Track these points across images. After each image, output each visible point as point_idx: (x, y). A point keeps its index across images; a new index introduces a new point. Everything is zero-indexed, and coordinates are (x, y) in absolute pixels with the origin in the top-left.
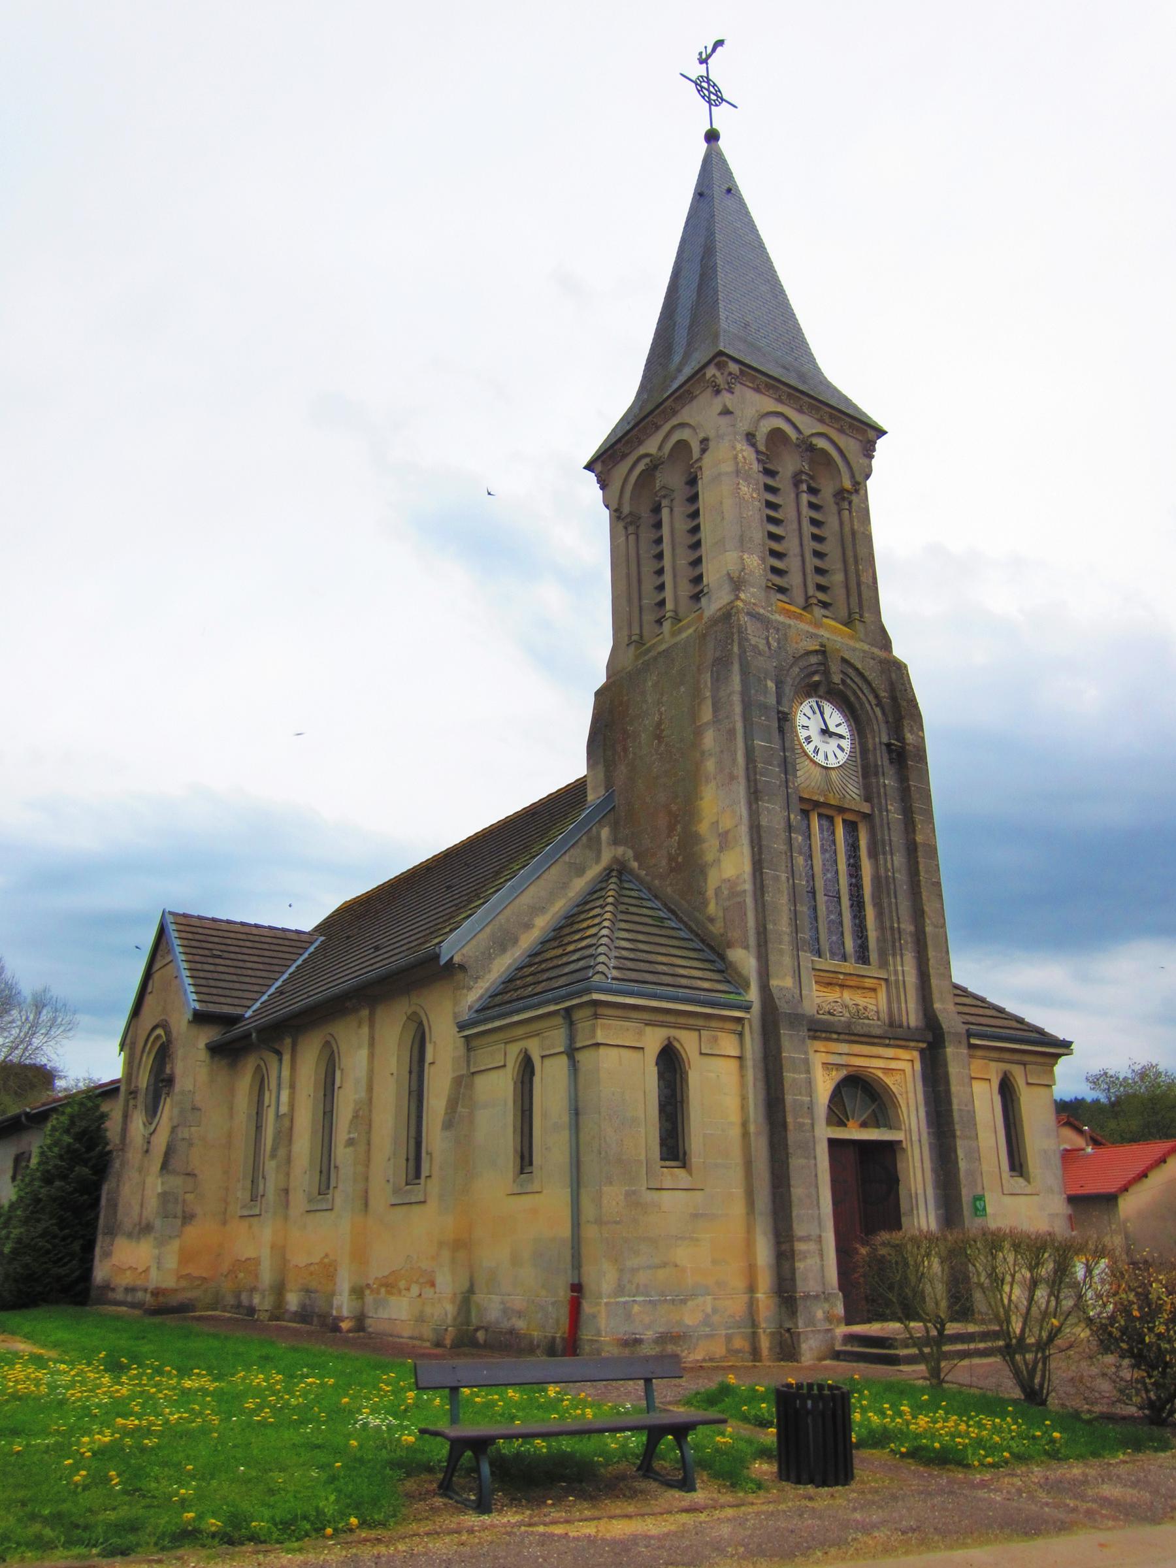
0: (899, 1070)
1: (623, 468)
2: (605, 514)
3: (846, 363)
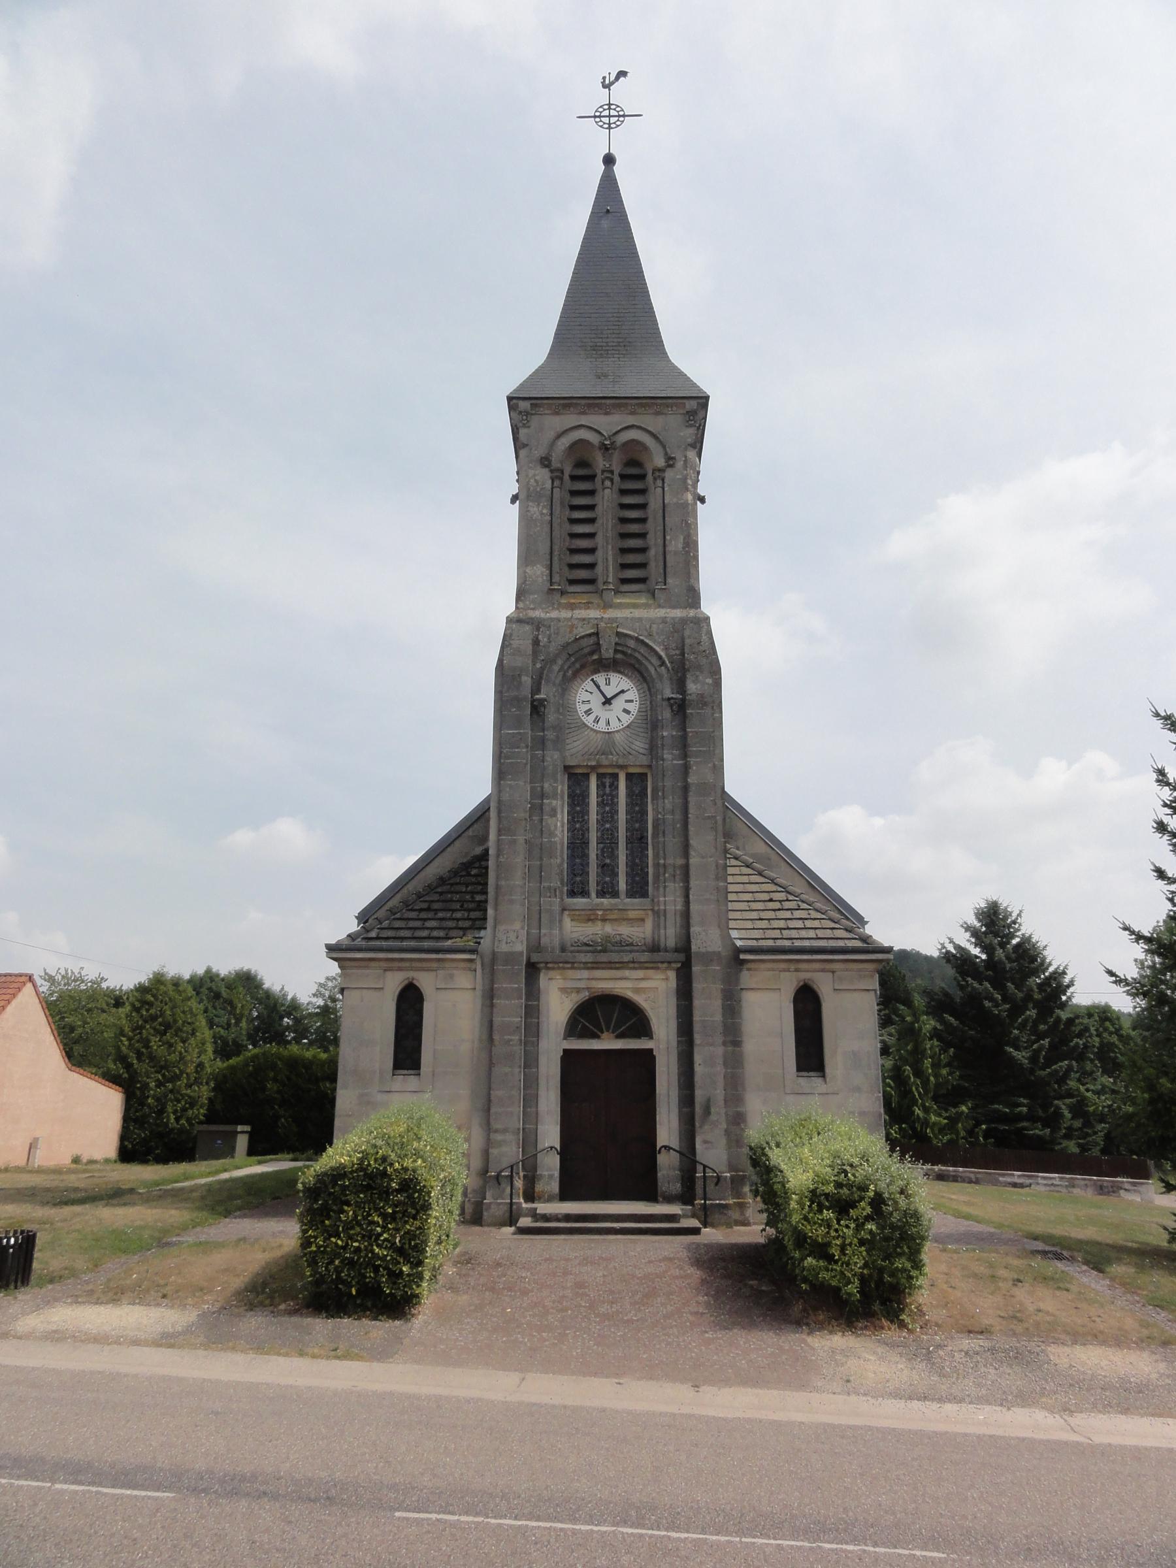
0: (653, 991)
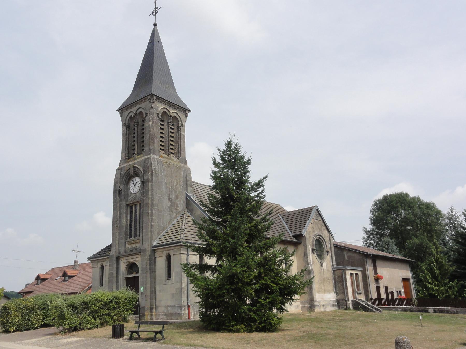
1: (126, 113)
2: (121, 123)
3: (184, 92)
